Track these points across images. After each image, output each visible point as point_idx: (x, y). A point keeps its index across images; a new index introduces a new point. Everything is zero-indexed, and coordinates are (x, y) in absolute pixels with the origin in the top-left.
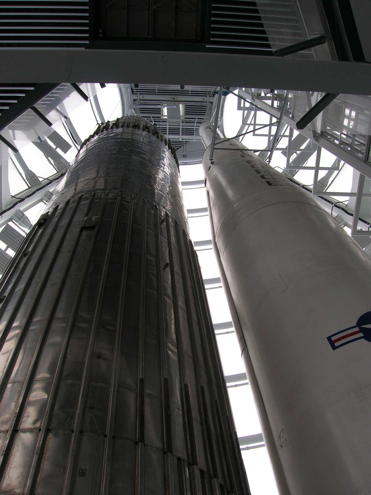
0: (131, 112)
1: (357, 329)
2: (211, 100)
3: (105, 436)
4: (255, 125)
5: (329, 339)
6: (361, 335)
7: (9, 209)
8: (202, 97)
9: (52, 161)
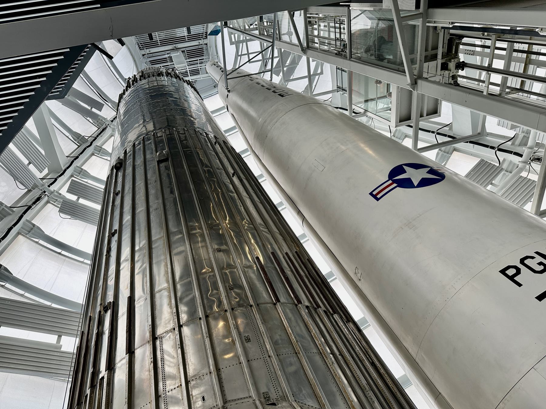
0: (144, 66)
1: (390, 182)
2: (205, 42)
3: (251, 306)
4: (248, 54)
5: (371, 194)
6: (395, 185)
7: (68, 168)
8: (197, 41)
9: (90, 120)
